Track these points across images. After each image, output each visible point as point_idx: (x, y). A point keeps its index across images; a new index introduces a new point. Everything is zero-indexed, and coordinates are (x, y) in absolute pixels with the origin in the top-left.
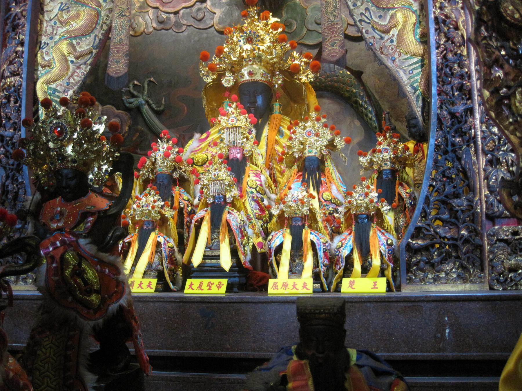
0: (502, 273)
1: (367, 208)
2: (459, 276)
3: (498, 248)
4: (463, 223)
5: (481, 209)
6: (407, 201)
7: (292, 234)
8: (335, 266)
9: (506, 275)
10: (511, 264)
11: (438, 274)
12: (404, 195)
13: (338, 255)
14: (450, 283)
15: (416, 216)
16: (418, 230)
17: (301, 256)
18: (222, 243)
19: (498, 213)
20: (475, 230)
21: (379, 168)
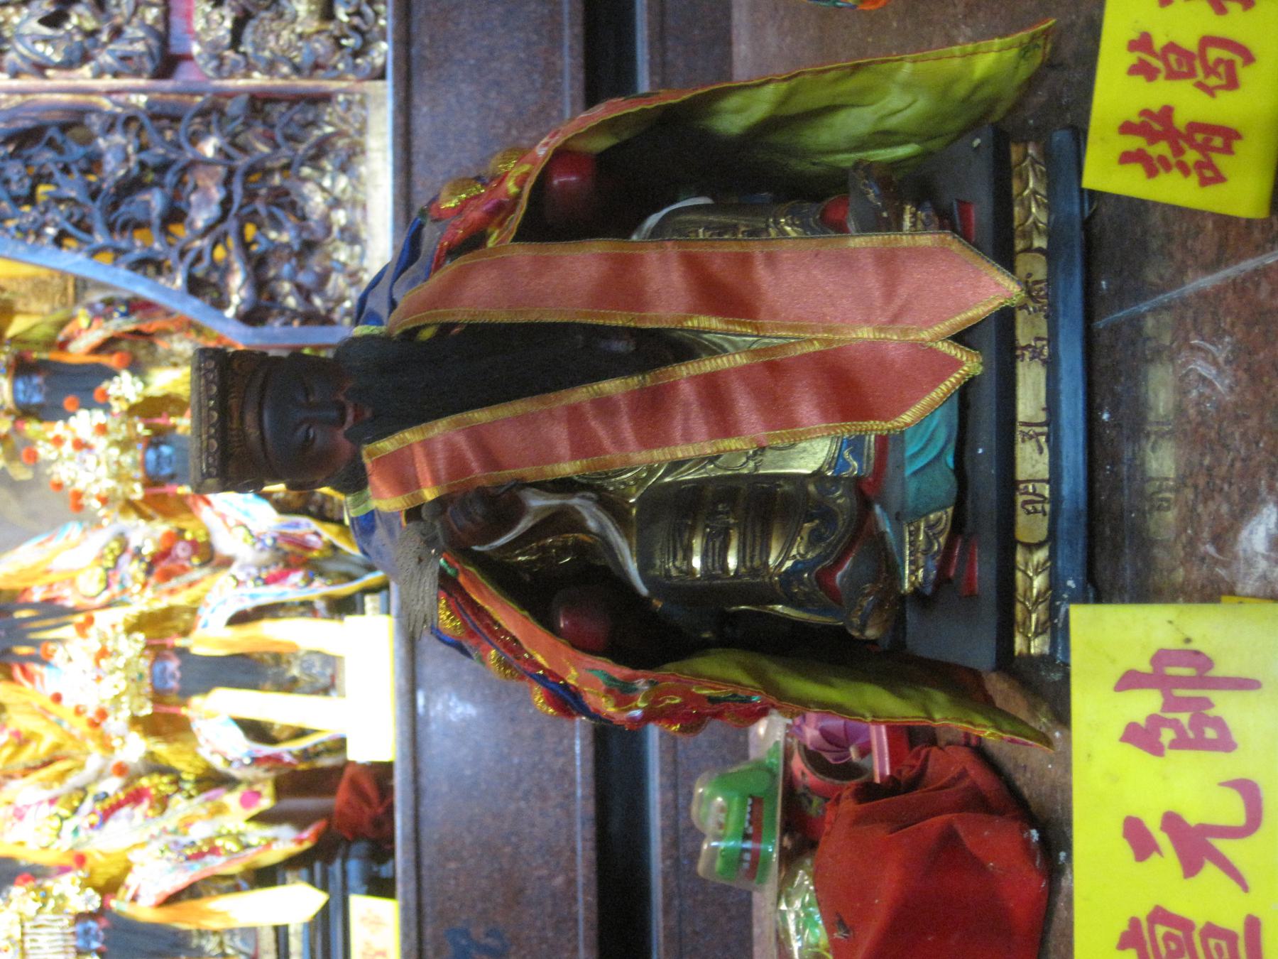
0: (337, 40)
1: (125, 445)
2: (344, 168)
3: (258, 47)
4: (179, 147)
5: (138, 93)
6: (119, 324)
7: (205, 689)
8: (310, 549)
9: (341, 29)
10: (310, 12)
11: (335, 229)
12: (96, 335)
13: (275, 539)
14: (365, 194)
15: (151, 289)
16: (195, 286)
17: (277, 657)
19: (153, 42)
20: (203, 113)
21: (9, 413)
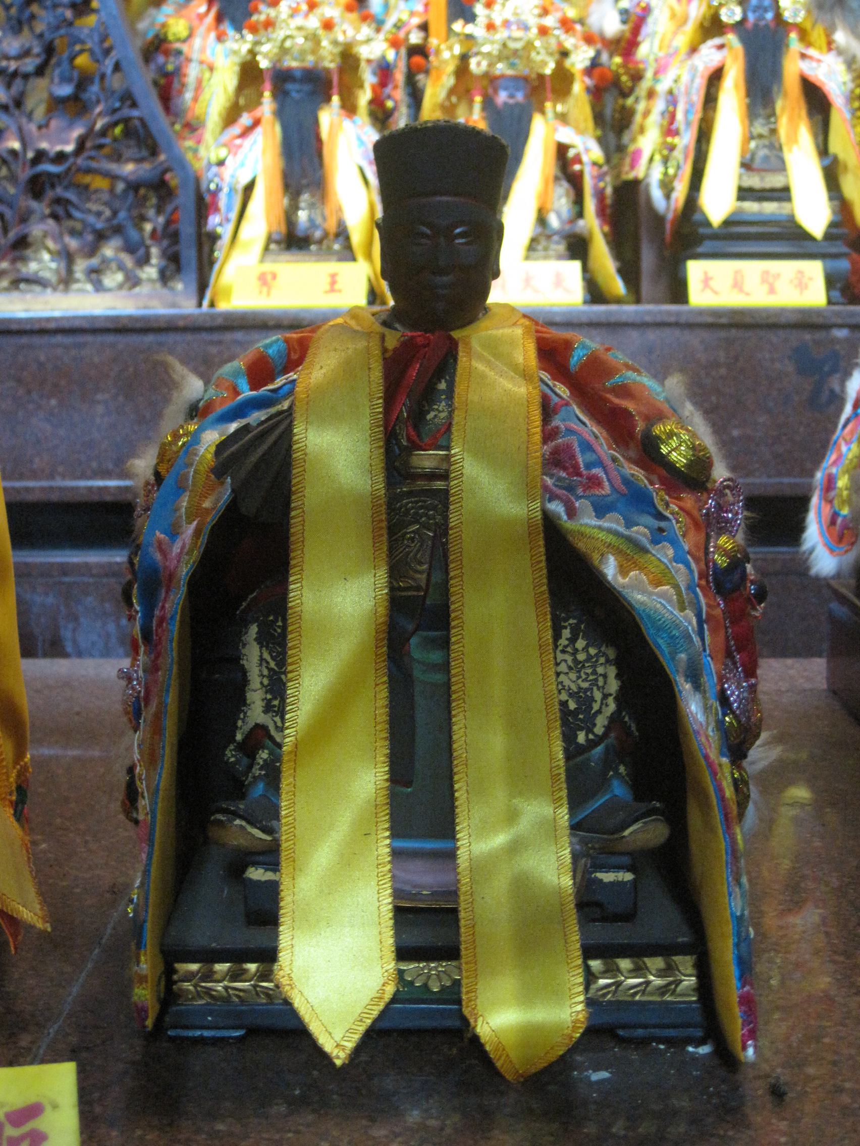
18: (790, 150)
